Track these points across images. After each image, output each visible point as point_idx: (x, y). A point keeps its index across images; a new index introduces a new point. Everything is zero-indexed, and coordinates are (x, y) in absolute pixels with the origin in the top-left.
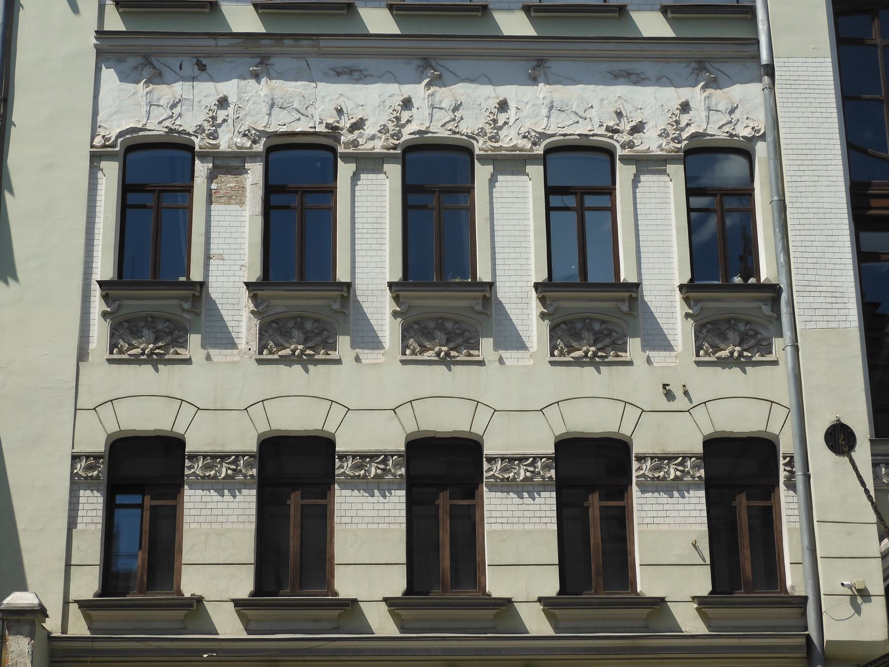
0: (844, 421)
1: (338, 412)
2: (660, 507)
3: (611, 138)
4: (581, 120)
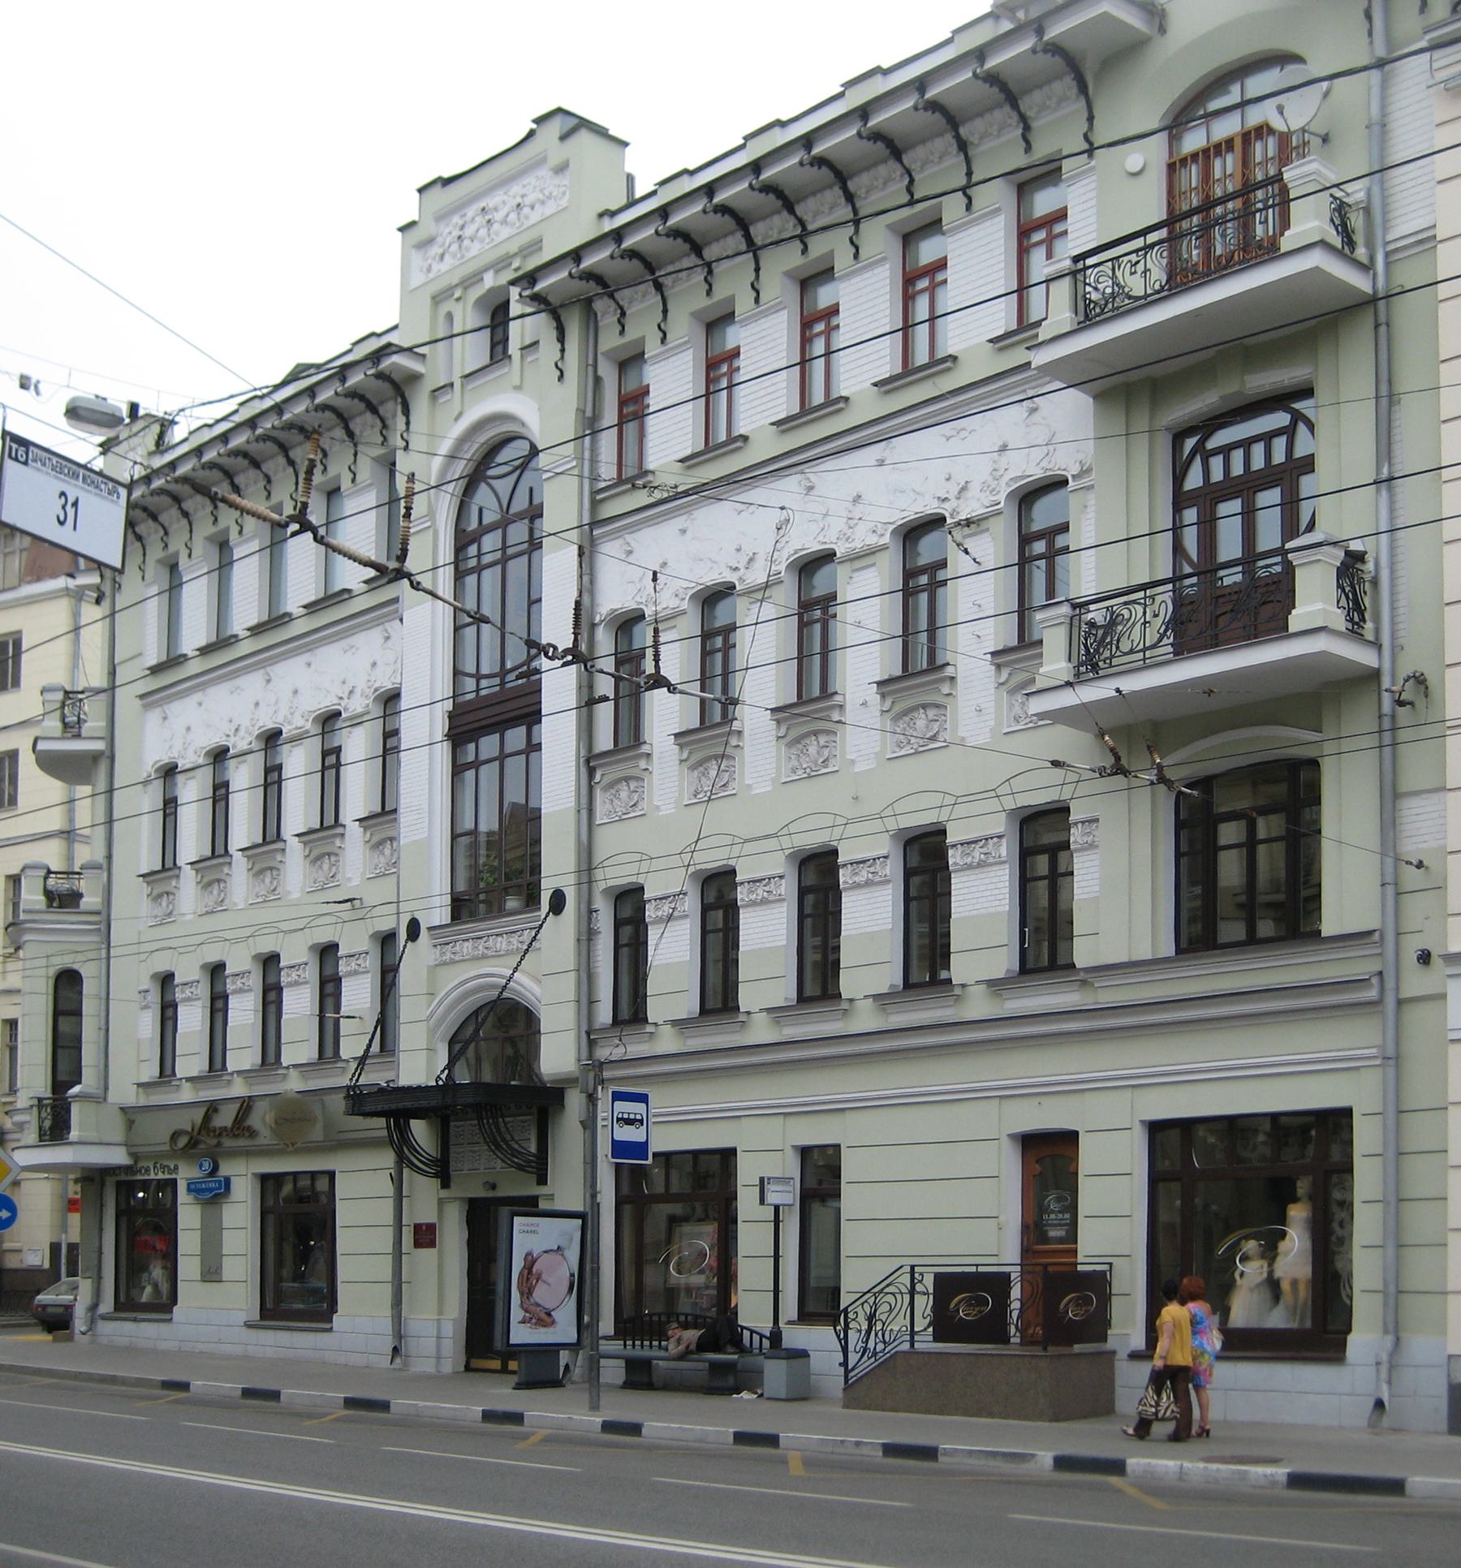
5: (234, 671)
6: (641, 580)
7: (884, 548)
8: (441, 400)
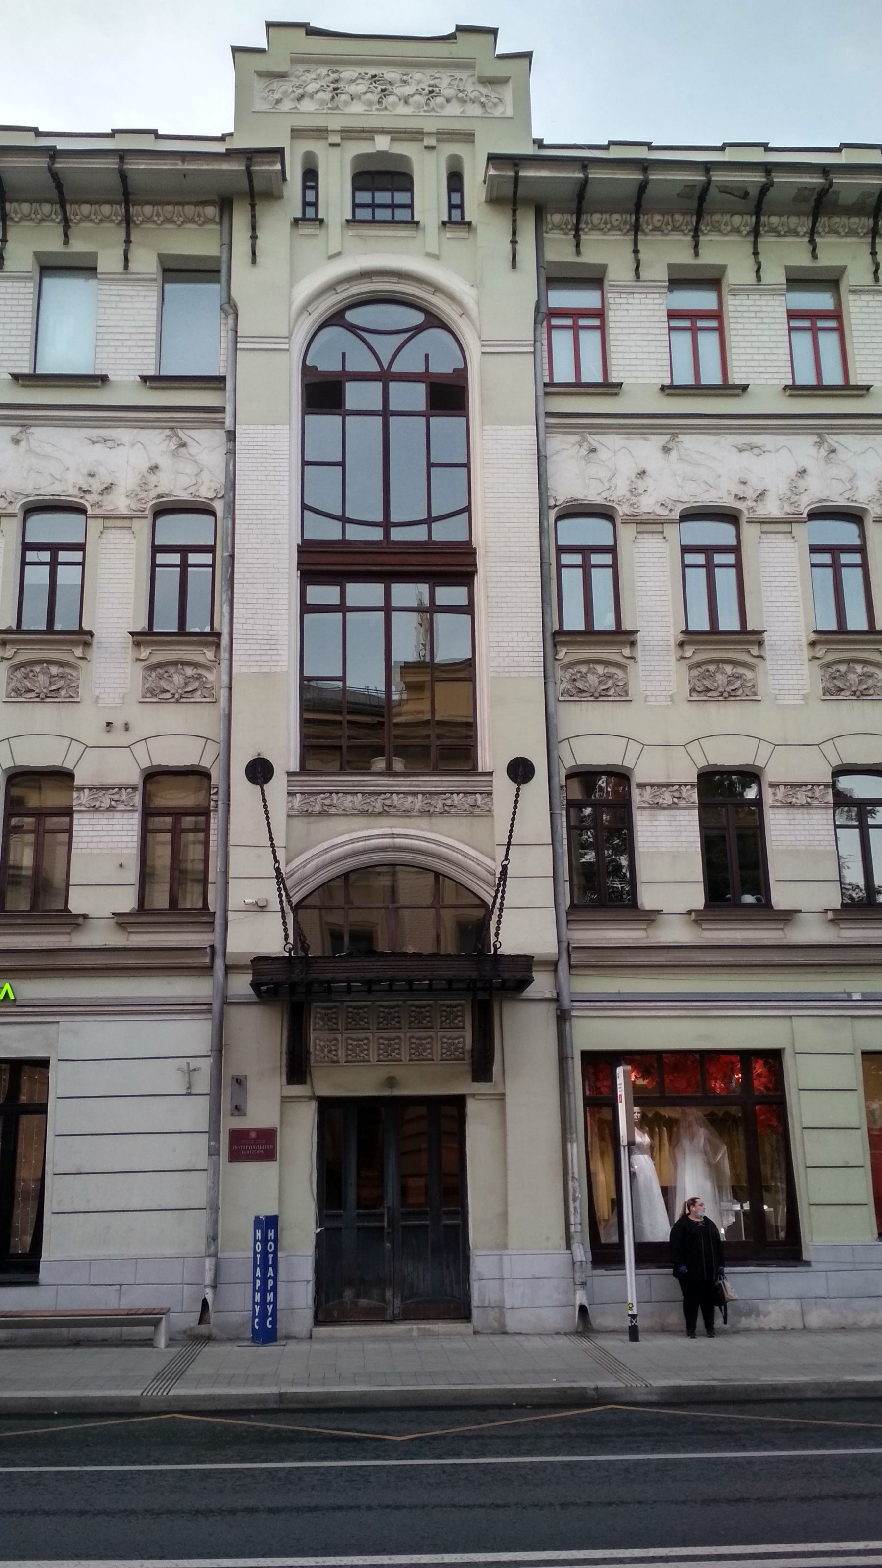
0: (263, 756)
1: (765, 749)
2: (96, 833)
3: (82, 498)
4: (57, 482)
5: (141, 420)
6: (610, 479)
7: (12, 516)
8: (301, 232)
